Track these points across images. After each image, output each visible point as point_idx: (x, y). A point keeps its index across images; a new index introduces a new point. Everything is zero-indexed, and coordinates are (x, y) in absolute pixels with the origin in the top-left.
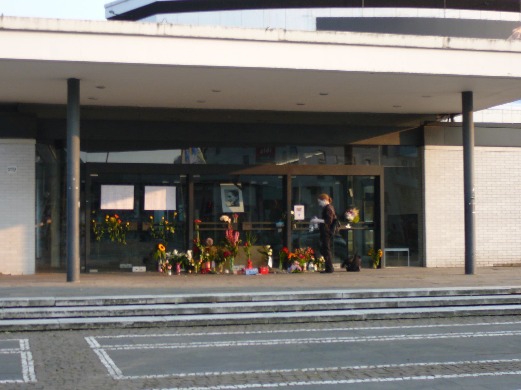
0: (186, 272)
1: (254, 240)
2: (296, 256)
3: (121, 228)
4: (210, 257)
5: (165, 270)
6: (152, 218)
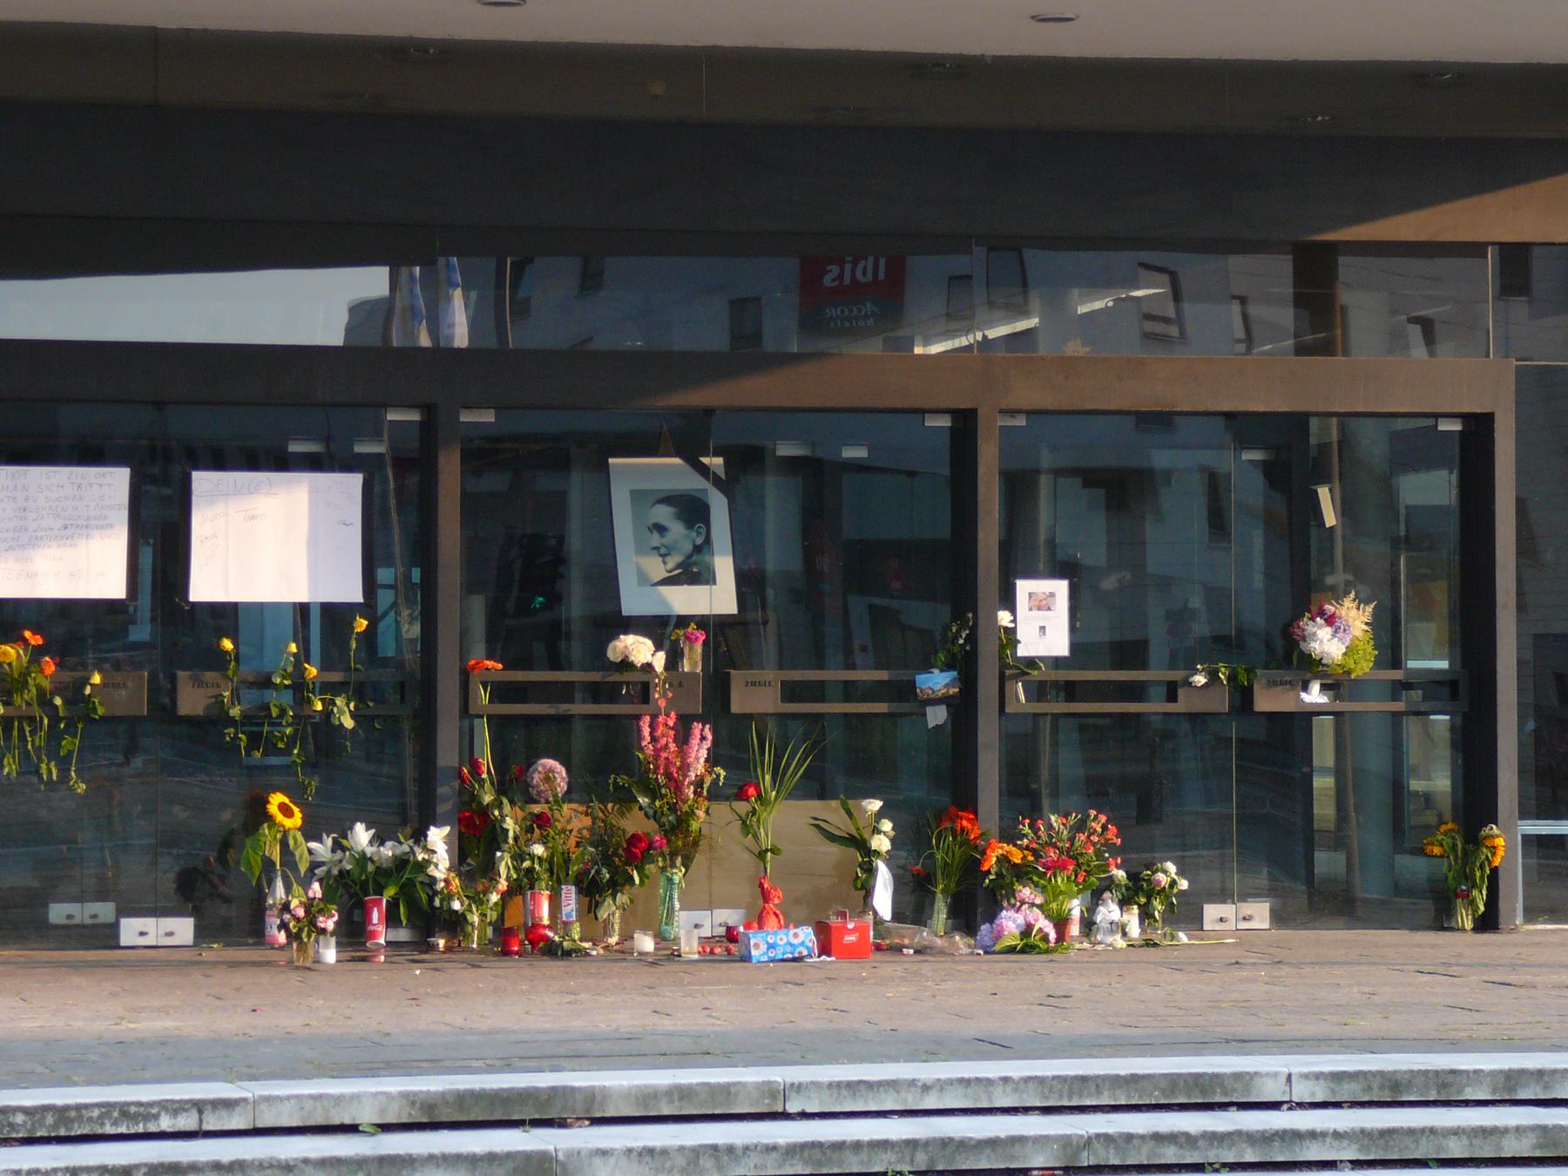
0: (422, 945)
1: (796, 772)
2: (1024, 858)
3: (58, 701)
4: (549, 862)
5: (304, 935)
6: (227, 644)
